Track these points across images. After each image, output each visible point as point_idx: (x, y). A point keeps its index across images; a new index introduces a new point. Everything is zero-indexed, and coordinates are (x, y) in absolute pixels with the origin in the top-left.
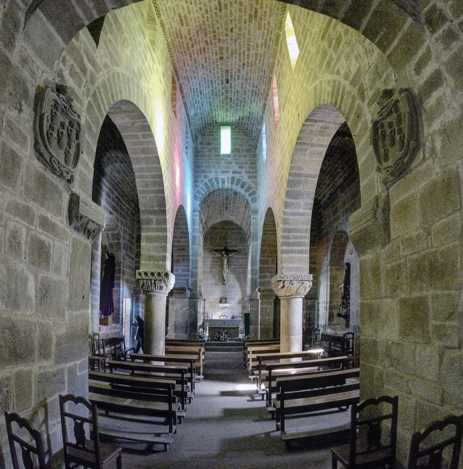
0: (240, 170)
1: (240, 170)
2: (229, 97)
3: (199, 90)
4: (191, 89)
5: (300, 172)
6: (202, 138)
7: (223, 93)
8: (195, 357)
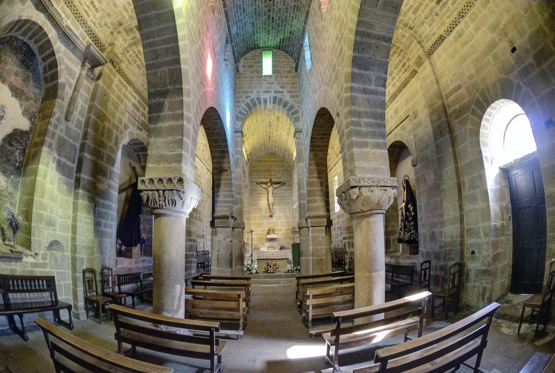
0: (281, 90)
1: (281, 90)
2: (271, 16)
3: (242, 7)
4: (234, 4)
5: (370, 31)
6: (244, 62)
7: (265, 12)
8: (233, 304)
